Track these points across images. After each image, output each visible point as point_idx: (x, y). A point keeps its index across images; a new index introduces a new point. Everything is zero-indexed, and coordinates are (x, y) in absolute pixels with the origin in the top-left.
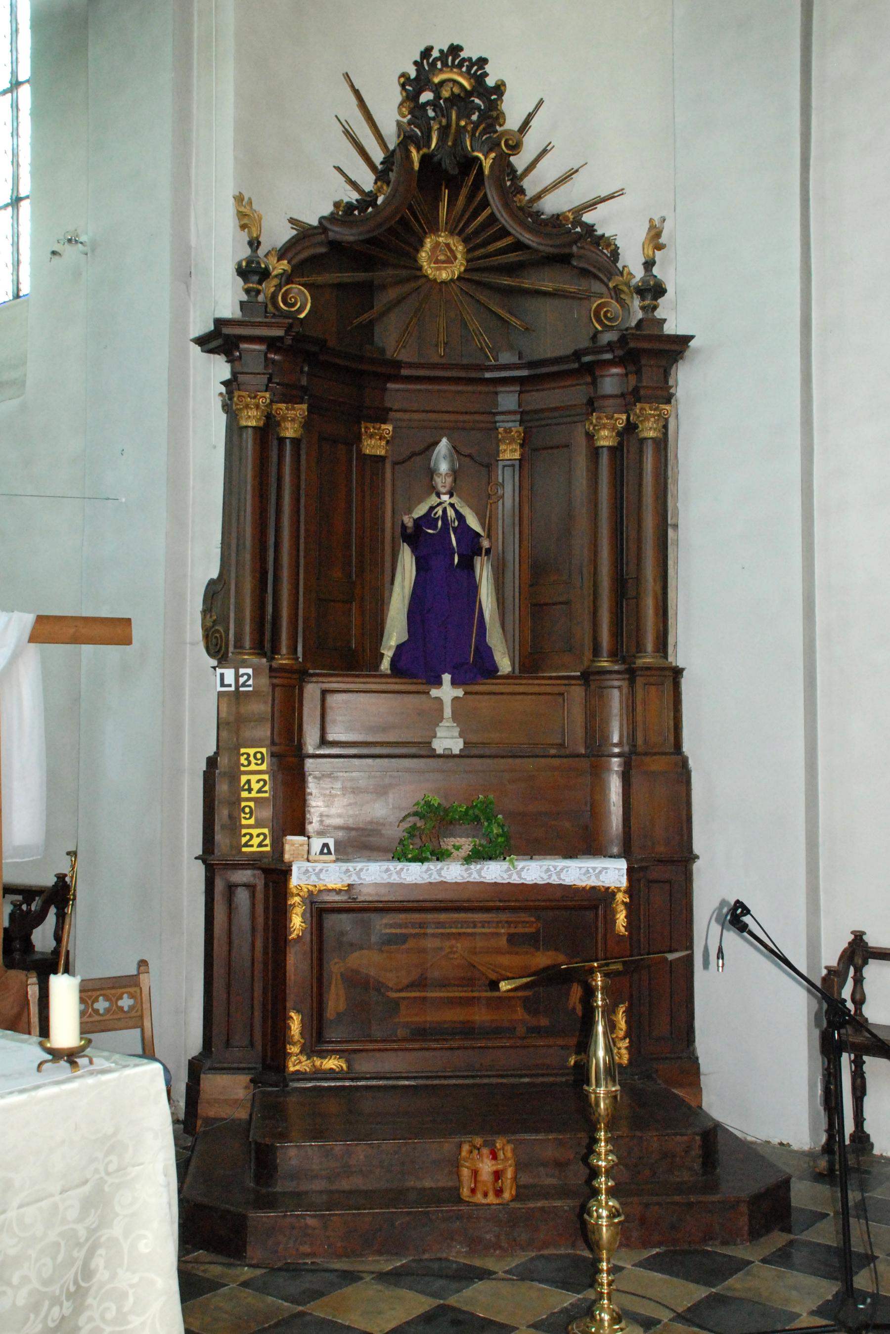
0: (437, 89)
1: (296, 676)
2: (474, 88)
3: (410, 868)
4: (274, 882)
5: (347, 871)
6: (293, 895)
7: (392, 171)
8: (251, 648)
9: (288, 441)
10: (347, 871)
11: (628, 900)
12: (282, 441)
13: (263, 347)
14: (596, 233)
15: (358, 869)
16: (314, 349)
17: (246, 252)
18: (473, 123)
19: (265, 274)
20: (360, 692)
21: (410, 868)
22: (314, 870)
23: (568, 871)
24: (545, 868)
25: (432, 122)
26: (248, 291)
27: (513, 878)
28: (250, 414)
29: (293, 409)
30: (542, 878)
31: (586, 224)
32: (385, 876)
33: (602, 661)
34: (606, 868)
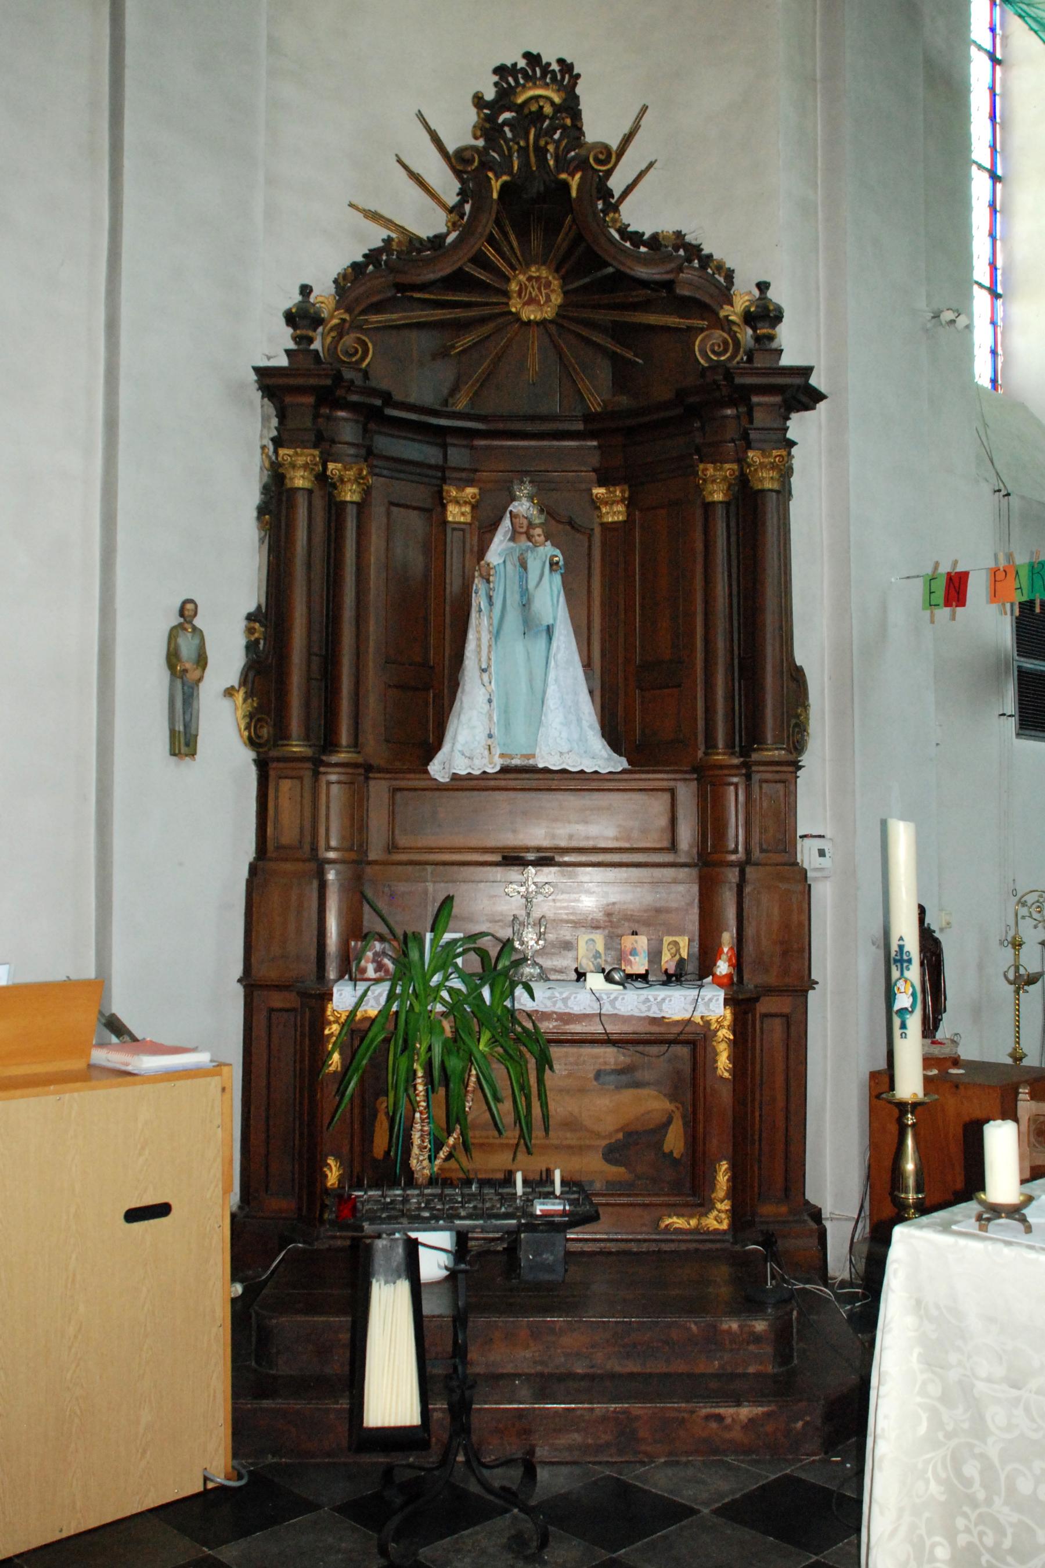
0: (519, 108)
1: (361, 771)
2: (565, 100)
3: (626, 997)
4: (311, 1008)
5: (647, 1000)
6: (330, 1023)
7: (468, 202)
8: (775, 743)
9: (349, 507)
10: (647, 1000)
11: (732, 1037)
12: (709, 507)
13: (310, 400)
14: (703, 252)
15: (659, 999)
16: (378, 402)
17: (297, 298)
18: (555, 141)
19: (317, 321)
20: (529, 790)
21: (626, 997)
22: (655, 999)
23: (670, 1000)
24: (642, 998)
25: (511, 143)
26: (296, 339)
27: (558, 1006)
28: (764, 475)
29: (721, 469)
30: (640, 1010)
31: (690, 244)
32: (549, 1003)
33: (292, 745)
34: (670, 996)
